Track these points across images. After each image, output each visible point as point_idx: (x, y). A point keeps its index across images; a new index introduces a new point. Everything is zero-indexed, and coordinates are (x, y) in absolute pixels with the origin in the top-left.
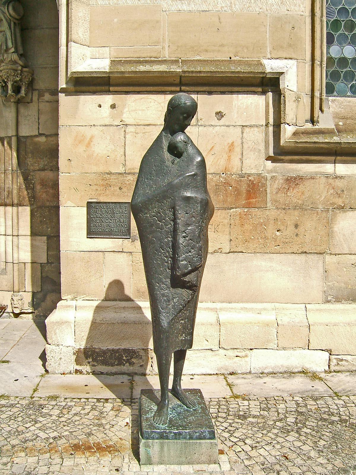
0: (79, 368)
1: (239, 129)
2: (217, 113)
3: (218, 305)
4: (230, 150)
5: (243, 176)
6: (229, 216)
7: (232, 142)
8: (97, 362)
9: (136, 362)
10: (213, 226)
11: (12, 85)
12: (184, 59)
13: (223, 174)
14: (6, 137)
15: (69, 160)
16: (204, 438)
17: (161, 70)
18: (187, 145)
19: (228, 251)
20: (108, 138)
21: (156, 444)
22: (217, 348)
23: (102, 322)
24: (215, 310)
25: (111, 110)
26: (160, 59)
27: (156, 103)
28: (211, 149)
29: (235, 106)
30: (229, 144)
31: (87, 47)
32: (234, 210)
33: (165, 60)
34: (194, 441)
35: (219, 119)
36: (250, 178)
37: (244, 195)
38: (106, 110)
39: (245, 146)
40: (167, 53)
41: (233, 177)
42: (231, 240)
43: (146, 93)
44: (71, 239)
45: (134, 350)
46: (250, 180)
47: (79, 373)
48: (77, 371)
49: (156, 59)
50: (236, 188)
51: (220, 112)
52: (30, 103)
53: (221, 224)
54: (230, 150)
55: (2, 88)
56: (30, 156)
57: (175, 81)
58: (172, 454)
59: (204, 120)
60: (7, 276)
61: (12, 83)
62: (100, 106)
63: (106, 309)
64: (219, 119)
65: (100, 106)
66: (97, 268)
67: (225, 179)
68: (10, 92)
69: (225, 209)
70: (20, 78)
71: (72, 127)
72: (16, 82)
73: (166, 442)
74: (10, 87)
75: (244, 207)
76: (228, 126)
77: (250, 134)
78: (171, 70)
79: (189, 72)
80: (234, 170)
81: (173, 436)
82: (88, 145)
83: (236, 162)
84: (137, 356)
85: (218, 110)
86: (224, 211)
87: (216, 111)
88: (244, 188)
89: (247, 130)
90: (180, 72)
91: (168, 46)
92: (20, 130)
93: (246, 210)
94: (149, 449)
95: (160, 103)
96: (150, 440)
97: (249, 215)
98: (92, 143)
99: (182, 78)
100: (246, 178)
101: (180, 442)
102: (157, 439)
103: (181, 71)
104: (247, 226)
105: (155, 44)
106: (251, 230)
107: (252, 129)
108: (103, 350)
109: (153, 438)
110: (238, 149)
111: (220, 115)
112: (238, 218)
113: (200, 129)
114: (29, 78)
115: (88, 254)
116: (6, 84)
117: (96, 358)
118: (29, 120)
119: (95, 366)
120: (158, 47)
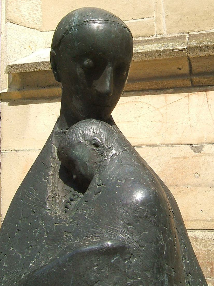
12: (195, 33)
17: (150, 49)
18: (102, 154)
26: (152, 38)
31: (38, 31)
33: (162, 39)
40: (165, 27)
43: (132, 93)
49: (146, 39)
57: (180, 69)
71: (19, 153)
79: (200, 48)
90: (183, 50)
91: (164, 16)
99: (192, 64)
103: (185, 47)
105: (144, 16)
120: (149, 19)
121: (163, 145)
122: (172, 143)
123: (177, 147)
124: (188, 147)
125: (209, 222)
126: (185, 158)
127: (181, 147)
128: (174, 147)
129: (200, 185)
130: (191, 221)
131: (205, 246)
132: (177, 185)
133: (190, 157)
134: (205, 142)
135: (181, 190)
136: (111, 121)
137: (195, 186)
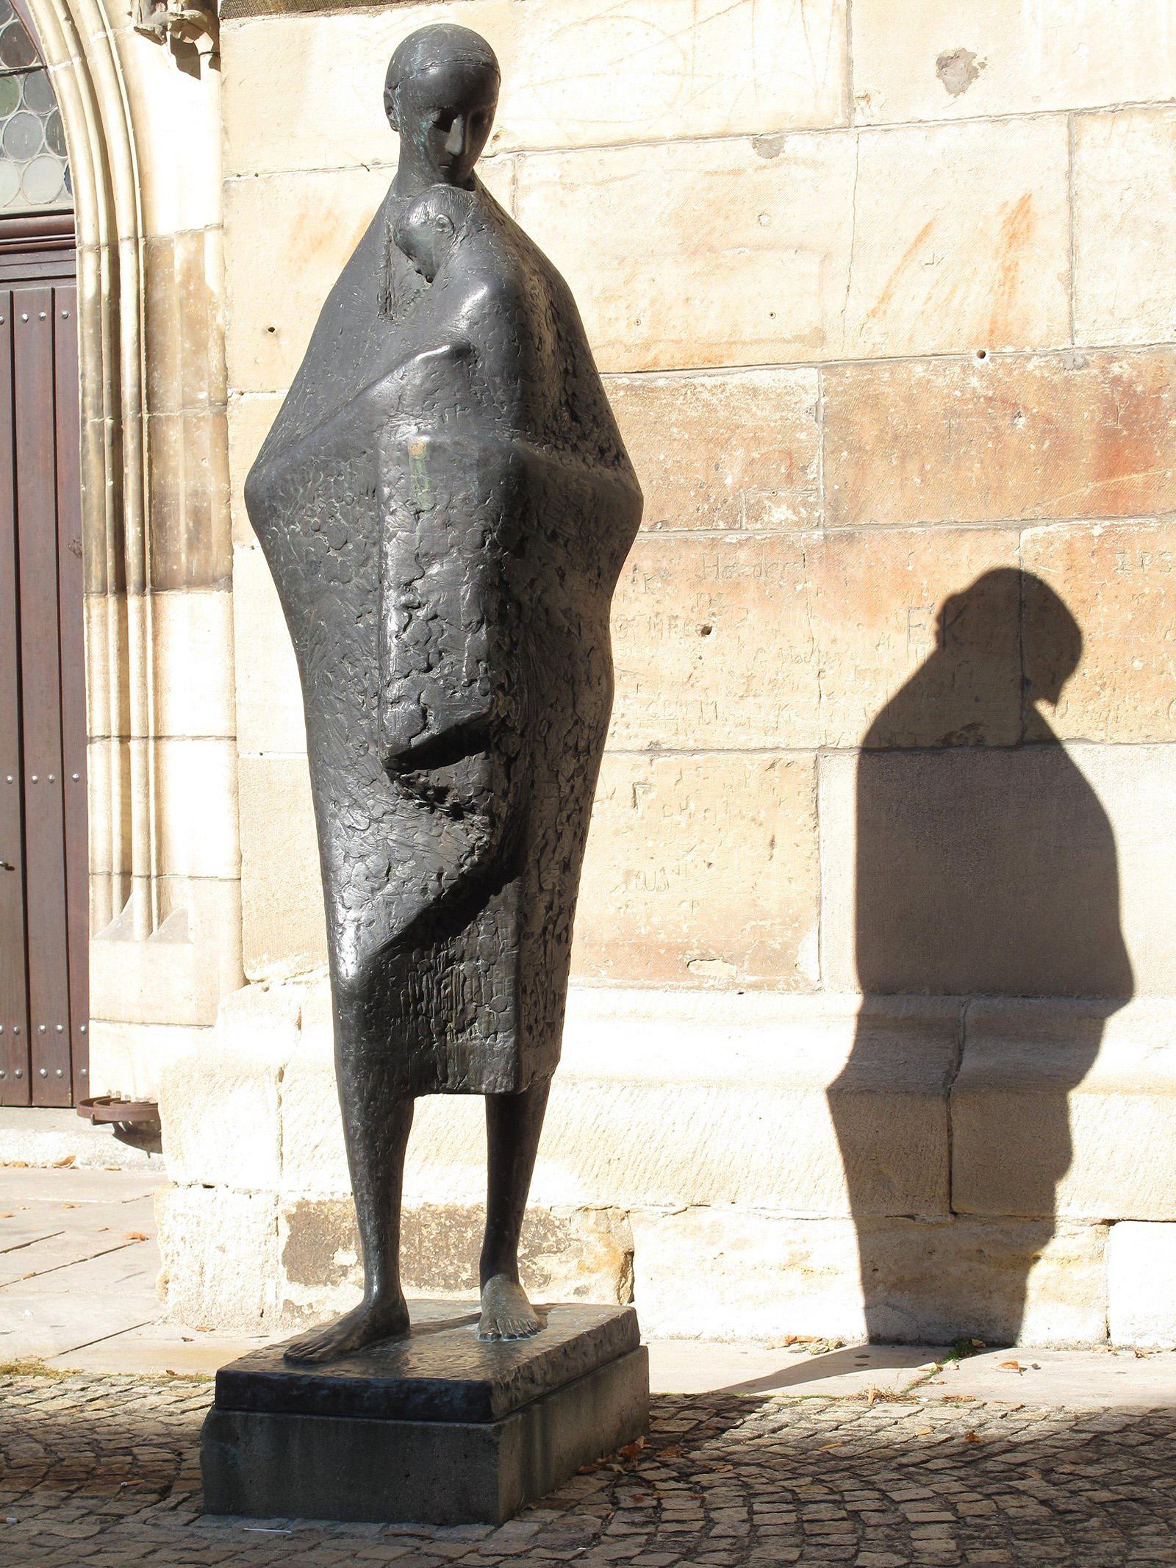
1: (1056, 131)
5: (1080, 361)
13: (982, 355)
15: (272, 330)
19: (1011, 737)
28: (920, 239)
30: (1008, 210)
32: (1040, 530)
35: (957, 90)
36: (1115, 369)
37: (1088, 456)
41: (1030, 366)
46: (1116, 380)
67: (992, 380)
75: (1089, 511)
76: (1000, 119)
80: (1037, 334)
84: (559, 1242)
85: (950, 47)
88: (1085, 421)
93: (1097, 531)
97: (1112, 550)
100: (1095, 371)
107: (1122, 125)
121: (682, 139)
122: (705, 132)
124: (745, 145)
125: (789, 342)
126: (737, 172)
127: (728, 143)
130: (744, 343)
131: (777, 408)
132: (711, 249)
134: (788, 126)
136: (470, 183)
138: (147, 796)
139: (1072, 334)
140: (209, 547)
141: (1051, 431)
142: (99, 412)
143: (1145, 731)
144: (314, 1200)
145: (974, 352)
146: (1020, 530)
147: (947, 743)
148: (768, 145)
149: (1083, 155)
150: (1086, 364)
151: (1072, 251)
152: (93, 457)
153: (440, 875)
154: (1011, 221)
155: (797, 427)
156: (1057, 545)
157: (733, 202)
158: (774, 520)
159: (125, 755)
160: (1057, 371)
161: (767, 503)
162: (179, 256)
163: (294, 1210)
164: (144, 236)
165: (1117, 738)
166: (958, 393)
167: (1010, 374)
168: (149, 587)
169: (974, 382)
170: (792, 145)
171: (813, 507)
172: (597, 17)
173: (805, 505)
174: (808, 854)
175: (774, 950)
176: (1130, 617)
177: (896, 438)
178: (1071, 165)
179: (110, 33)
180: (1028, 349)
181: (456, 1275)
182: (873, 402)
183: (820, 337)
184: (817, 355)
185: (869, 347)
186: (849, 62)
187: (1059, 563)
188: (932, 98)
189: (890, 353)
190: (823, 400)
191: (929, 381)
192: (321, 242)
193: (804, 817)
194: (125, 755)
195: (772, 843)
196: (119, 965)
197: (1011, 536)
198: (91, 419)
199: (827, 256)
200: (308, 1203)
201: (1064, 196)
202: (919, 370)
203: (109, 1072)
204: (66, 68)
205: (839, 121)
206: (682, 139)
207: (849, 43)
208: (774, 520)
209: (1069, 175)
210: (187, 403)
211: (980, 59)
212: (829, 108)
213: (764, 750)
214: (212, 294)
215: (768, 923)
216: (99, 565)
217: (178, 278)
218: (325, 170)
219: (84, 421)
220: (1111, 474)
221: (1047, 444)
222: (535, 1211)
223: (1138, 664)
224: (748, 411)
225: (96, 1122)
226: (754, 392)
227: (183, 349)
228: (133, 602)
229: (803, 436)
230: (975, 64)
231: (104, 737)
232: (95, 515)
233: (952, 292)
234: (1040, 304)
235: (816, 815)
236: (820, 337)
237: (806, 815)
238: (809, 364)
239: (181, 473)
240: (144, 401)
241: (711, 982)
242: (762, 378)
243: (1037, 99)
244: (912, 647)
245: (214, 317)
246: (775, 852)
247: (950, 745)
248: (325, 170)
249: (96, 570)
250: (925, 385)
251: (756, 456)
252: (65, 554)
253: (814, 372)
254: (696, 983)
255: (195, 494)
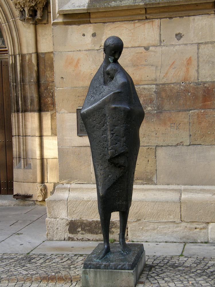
0: (71, 236)
1: (196, 47)
2: (176, 35)
3: (183, 187)
4: (188, 64)
5: (199, 84)
6: (188, 116)
7: (189, 57)
8: (85, 231)
9: (115, 231)
10: (176, 124)
11: (29, 10)
13: (183, 83)
14: (28, 54)
15: (62, 78)
16: (125, 269)
19: (188, 144)
20: (91, 60)
21: (91, 272)
22: (179, 221)
23: (88, 200)
24: (180, 191)
25: (92, 38)
27: (127, 30)
28: (172, 64)
29: (192, 27)
30: (187, 59)
32: (193, 111)
34: (117, 271)
35: (178, 39)
36: (205, 85)
37: (201, 99)
38: (89, 38)
39: (201, 60)
41: (191, 85)
42: (190, 135)
44: (65, 138)
45: (113, 222)
46: (206, 87)
47: (71, 240)
48: (70, 239)
50: (194, 94)
51: (179, 34)
52: (46, 24)
53: (182, 123)
54: (188, 64)
55: (21, 12)
56: (49, 69)
58: (102, 279)
59: (165, 41)
60: (32, 170)
61: (28, 8)
62: (84, 35)
63: (93, 190)
64: (178, 39)
65: (84, 35)
66: (85, 159)
67: (185, 87)
68: (27, 16)
69: (185, 111)
70: (35, 4)
72: (33, 7)
73: (98, 271)
74: (27, 12)
75: (201, 108)
76: (186, 45)
77: (205, 50)
78: (135, 4)
80: (192, 80)
81: (103, 267)
82: (77, 65)
83: (193, 73)
84: (115, 226)
85: (178, 32)
86: (184, 113)
87: (176, 33)
88: (200, 93)
89: (202, 46)
92: (39, 47)
93: (202, 111)
94: (87, 276)
95: (130, 30)
96: (88, 269)
97: (205, 114)
98: (79, 65)
100: (202, 86)
101: (107, 271)
102: (93, 268)
104: (203, 124)
106: (207, 127)
107: (207, 45)
108: (89, 221)
109: (90, 268)
110: (195, 63)
111: (179, 36)
112: (196, 117)
113: (163, 48)
114: (43, 3)
115: (79, 149)
116: (23, 9)
117: (84, 227)
118: (46, 39)
119: (84, 234)
121: (132, 47)
122: (136, 46)
123: (138, 48)
124: (143, 48)
125: (150, 81)
126: (142, 53)
127: (140, 48)
128: (137, 48)
129: (147, 65)
130: (143, 81)
131: (148, 91)
132: (137, 66)
133: (144, 53)
134: (150, 45)
135: (139, 67)
136: (118, 63)
137: (145, 65)
138: (24, 145)
139: (198, 79)
140: (34, 105)
141: (194, 95)
142: (13, 83)
143: (211, 143)
144: (74, 220)
145: (182, 83)
146: (190, 111)
147: (177, 145)
148: (147, 49)
149: (200, 50)
150: (200, 85)
151: (198, 66)
152: (12, 90)
153: (116, 177)
154: (188, 61)
155: (152, 94)
156: (196, 113)
157: (141, 58)
158: (148, 109)
159: (19, 138)
160: (196, 85)
161: (147, 107)
162: (27, 58)
163: (70, 222)
164: (21, 54)
165: (206, 144)
166: (179, 89)
167: (188, 86)
168: (23, 111)
169: (182, 87)
170: (151, 48)
171: (155, 107)
172: (117, 27)
173: (153, 107)
174: (154, 163)
175: (149, 178)
176: (208, 125)
177: (168, 96)
178: (198, 52)
179: (13, 19)
180: (191, 82)
181: (98, 232)
182: (165, 90)
183: (156, 80)
184: (155, 83)
185: (164, 82)
186: (160, 35)
187: (196, 116)
188: (175, 41)
189: (168, 82)
190: (156, 90)
191: (174, 87)
192: (70, 63)
193: (154, 157)
194: (19, 138)
195: (148, 161)
196: (18, 173)
197: (188, 112)
198: (12, 84)
199: (157, 67)
200: (73, 220)
201: (197, 57)
202: (172, 85)
203: (17, 189)
204: (5, 25)
205: (159, 44)
206: (132, 47)
207: (160, 32)
208: (148, 109)
209: (198, 54)
210: (30, 82)
211: (183, 34)
212: (157, 42)
213: (147, 146)
214: (34, 64)
215: (148, 174)
216: (14, 107)
217: (27, 61)
218: (71, 51)
219: (11, 84)
220: (205, 102)
221: (194, 97)
222: (111, 221)
223: (209, 133)
224: (144, 92)
225: (17, 199)
226: (145, 89)
227: (28, 73)
228: (20, 114)
229: (153, 96)
230: (182, 35)
231: (15, 136)
232: (13, 99)
233: (178, 73)
234: (193, 73)
235: (156, 156)
236: (156, 80)
237: (154, 157)
238: (154, 84)
239: (29, 93)
240: (22, 81)
241: (138, 183)
242: (146, 86)
243: (192, 41)
244: (171, 130)
245: (34, 68)
246: (149, 162)
247: (178, 145)
248: (71, 51)
249: (13, 108)
250: (173, 88)
251: (145, 99)
252: (10, 106)
253: (155, 86)
254: (136, 183)
255: (31, 96)
